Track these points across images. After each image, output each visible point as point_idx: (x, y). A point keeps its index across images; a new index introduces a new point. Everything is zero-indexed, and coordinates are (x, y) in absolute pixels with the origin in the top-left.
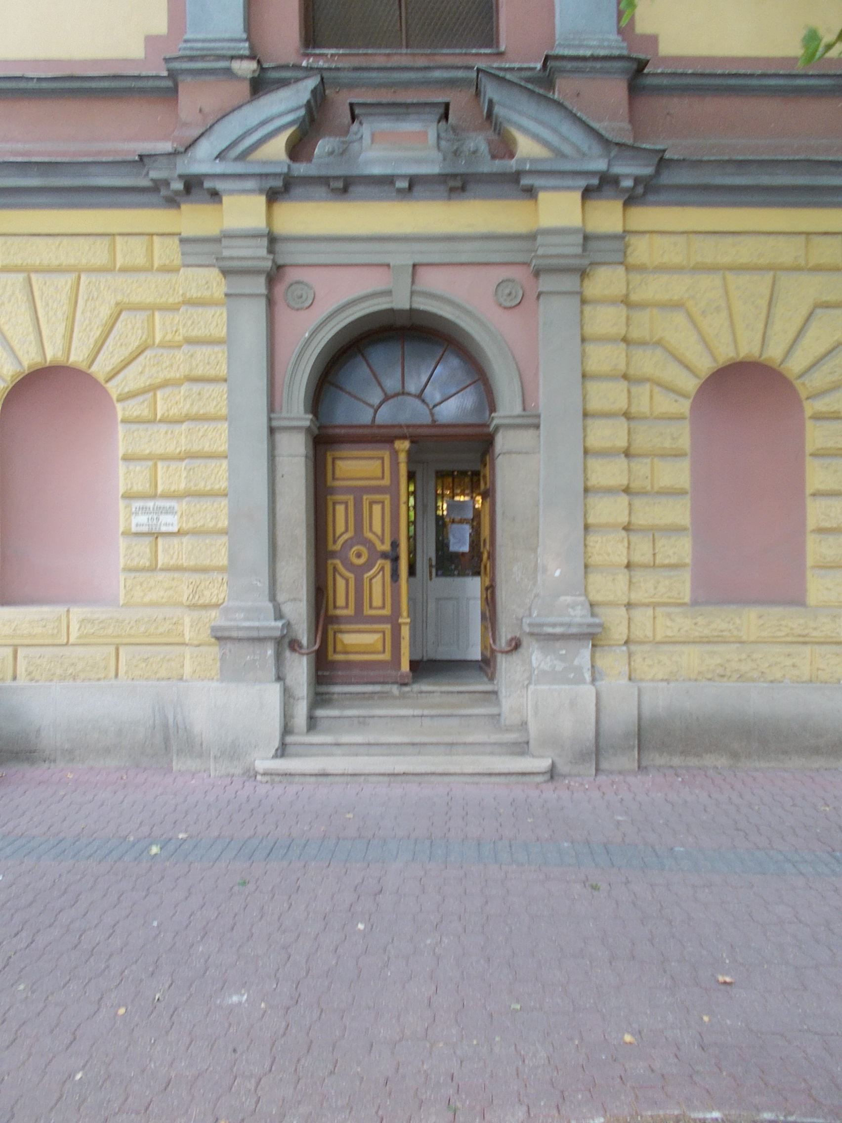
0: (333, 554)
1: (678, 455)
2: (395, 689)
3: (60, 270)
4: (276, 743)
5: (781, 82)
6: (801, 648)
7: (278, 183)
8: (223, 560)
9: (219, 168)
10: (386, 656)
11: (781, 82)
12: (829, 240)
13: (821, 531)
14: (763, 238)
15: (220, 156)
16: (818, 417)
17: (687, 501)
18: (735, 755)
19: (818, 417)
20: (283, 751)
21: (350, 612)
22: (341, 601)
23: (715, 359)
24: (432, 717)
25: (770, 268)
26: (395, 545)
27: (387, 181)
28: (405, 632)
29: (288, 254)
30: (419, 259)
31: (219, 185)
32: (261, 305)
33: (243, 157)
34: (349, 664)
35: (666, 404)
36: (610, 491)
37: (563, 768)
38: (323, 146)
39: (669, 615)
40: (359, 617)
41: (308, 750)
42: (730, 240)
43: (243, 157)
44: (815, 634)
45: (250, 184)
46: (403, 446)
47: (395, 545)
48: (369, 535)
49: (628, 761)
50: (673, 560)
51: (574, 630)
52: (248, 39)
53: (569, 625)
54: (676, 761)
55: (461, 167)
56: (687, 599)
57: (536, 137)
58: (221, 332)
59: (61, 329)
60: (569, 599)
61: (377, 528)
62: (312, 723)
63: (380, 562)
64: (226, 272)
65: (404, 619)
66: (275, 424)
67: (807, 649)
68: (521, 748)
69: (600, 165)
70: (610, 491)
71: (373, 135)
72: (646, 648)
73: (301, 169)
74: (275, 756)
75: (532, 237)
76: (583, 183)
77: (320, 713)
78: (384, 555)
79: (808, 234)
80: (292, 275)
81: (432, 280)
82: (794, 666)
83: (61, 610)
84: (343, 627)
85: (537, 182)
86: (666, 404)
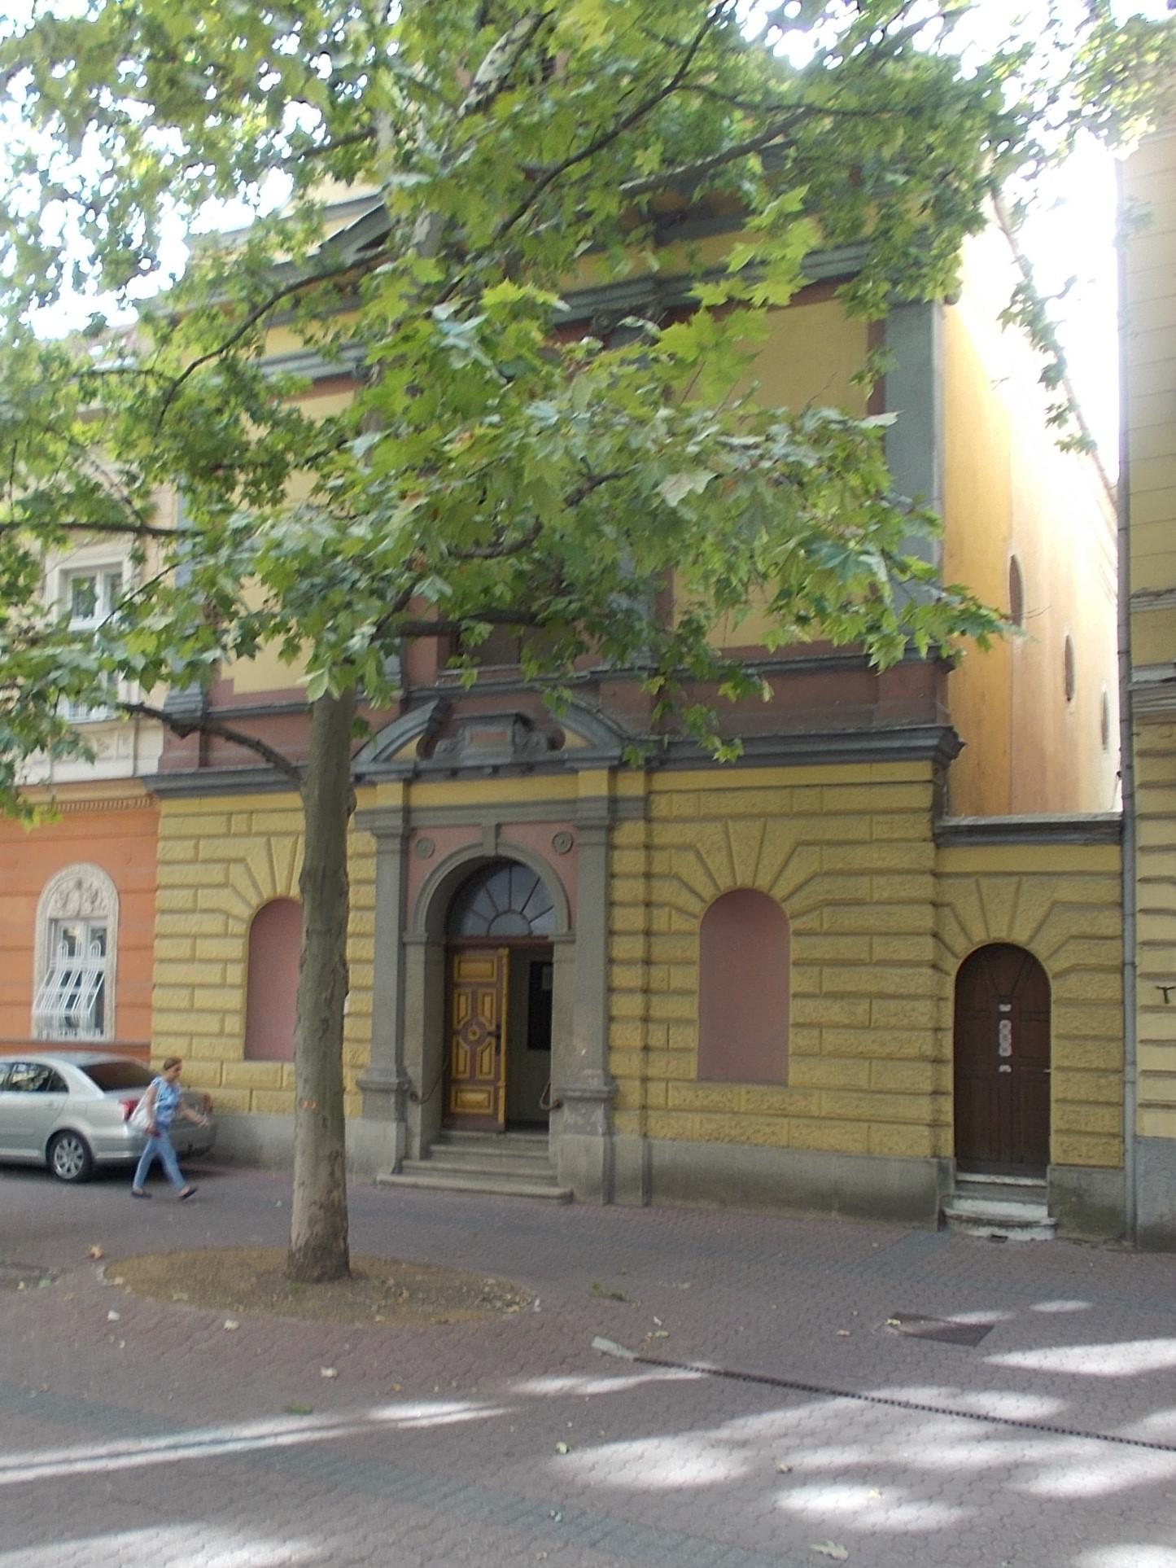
0: (457, 1033)
1: (688, 963)
2: (494, 1136)
3: (286, 834)
4: (393, 1164)
5: (777, 667)
6: (780, 1120)
7: (409, 775)
8: (369, 1035)
9: (373, 768)
10: (489, 1111)
11: (777, 667)
12: (808, 792)
13: (797, 1025)
14: (754, 792)
15: (375, 759)
16: (799, 933)
17: (696, 999)
18: (723, 1202)
19: (799, 933)
20: (399, 1169)
21: (467, 1075)
22: (461, 1068)
23: (239, 986)
24: (508, 1156)
25: (758, 816)
26: (498, 1027)
27: (479, 768)
28: (502, 1093)
29: (417, 820)
30: (502, 820)
31: (374, 778)
32: (397, 859)
33: (389, 758)
34: (466, 1115)
35: (679, 923)
36: (630, 991)
37: (578, 1195)
38: (440, 746)
39: (677, 1088)
40: (472, 1079)
41: (417, 1171)
42: (729, 795)
43: (389, 758)
44: (792, 1108)
45: (393, 776)
46: (505, 952)
47: (498, 1027)
48: (481, 1019)
49: (637, 1198)
50: (681, 1045)
51: (588, 1095)
52: (402, 672)
53: (584, 1091)
54: (678, 1203)
55: (524, 758)
56: (693, 1075)
57: (576, 732)
58: (373, 875)
59: (285, 873)
60: (589, 1072)
61: (487, 1013)
62: (426, 1154)
63: (489, 1039)
64: (379, 836)
65: (502, 1083)
66: (406, 940)
67: (786, 1121)
68: (552, 1181)
69: (617, 752)
70: (630, 991)
71: (472, 738)
72: (661, 1113)
73: (424, 765)
74: (393, 1172)
75: (573, 802)
76: (608, 764)
77: (434, 1148)
78: (490, 1034)
79: (793, 787)
80: (421, 834)
81: (512, 835)
82: (773, 1133)
83: (279, 1065)
84: (463, 1087)
85: (576, 765)
86: (679, 923)
